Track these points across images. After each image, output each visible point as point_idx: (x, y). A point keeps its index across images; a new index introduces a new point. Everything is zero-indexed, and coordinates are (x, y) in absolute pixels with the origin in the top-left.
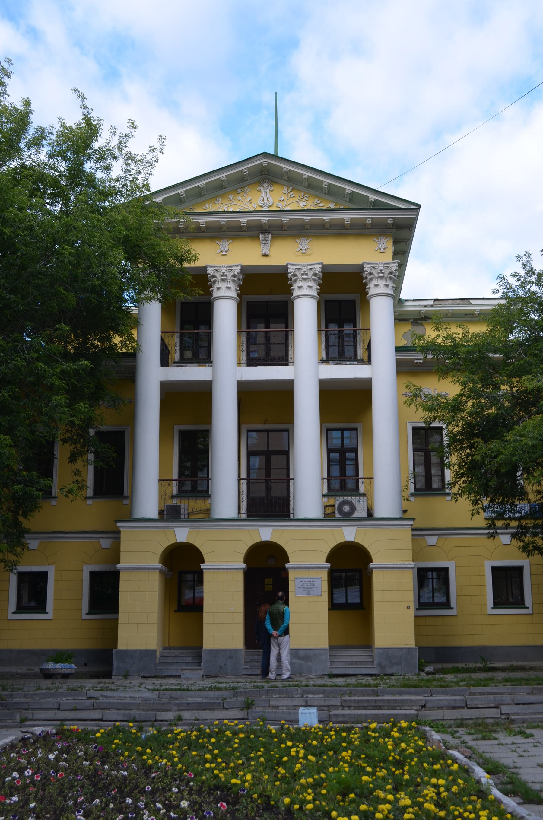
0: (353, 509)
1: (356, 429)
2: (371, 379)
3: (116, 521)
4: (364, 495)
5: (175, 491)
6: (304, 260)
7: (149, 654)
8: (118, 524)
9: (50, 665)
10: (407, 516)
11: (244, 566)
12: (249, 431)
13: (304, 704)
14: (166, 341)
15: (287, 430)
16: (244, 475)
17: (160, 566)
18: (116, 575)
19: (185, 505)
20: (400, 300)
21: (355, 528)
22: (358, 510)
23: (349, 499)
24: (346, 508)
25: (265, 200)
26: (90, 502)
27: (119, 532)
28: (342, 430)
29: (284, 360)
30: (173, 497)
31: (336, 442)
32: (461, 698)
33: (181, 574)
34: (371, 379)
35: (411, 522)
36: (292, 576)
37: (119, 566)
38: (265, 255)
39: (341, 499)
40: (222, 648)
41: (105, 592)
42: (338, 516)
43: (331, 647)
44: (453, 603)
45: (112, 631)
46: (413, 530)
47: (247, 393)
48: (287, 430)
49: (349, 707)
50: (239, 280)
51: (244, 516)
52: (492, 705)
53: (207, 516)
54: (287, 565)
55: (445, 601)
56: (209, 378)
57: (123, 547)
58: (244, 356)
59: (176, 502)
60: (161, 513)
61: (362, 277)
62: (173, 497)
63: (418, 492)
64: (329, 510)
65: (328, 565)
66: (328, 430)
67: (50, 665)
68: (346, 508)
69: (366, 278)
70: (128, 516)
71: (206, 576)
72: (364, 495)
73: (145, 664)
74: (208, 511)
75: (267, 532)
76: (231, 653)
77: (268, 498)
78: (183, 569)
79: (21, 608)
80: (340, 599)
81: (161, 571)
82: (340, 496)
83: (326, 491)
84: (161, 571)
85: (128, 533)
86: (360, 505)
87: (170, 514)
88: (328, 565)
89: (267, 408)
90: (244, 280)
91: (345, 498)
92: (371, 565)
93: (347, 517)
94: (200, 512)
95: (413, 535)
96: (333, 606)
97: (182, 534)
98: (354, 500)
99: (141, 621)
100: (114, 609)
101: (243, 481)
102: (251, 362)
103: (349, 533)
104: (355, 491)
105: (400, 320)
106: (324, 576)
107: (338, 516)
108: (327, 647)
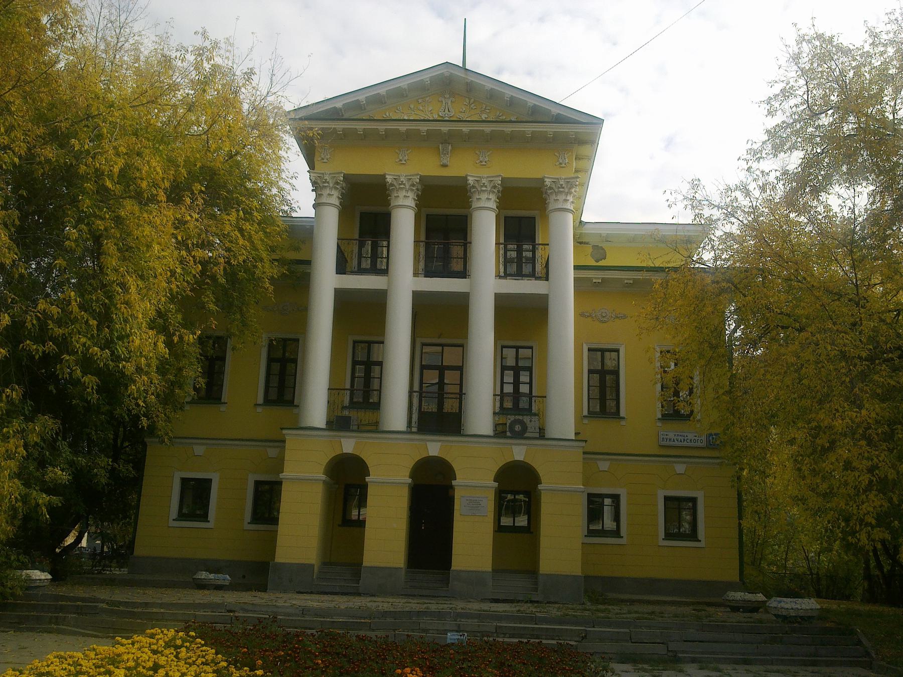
0: (525, 428)
1: (531, 348)
2: (547, 295)
3: (282, 429)
4: (535, 415)
5: (347, 402)
6: (485, 173)
7: (305, 568)
8: (284, 432)
9: (203, 575)
10: (580, 437)
11: (410, 481)
12: (423, 345)
13: (456, 628)
14: (342, 248)
15: (462, 346)
16: (416, 387)
17: (323, 477)
18: (279, 483)
19: (355, 415)
20: (581, 222)
21: (525, 447)
22: (529, 429)
23: (520, 418)
24: (518, 428)
25: (447, 111)
26: (259, 410)
27: (284, 441)
28: (517, 348)
29: (463, 274)
30: (344, 408)
31: (511, 362)
32: (628, 631)
33: (348, 487)
34: (547, 295)
35: (583, 444)
36: (458, 495)
37: (281, 476)
38: (445, 166)
39: (512, 418)
40: (382, 565)
41: (266, 501)
42: (508, 434)
43: (495, 571)
44: (624, 531)
45: (271, 541)
46: (584, 453)
47: (423, 305)
48: (462, 346)
49: (505, 634)
50: (418, 190)
51: (414, 430)
52: (658, 641)
53: (375, 427)
54: (454, 483)
55: (435, 410)
56: (385, 287)
57: (287, 457)
58: (422, 265)
59: (346, 413)
60: (329, 423)
61: (542, 192)
62: (344, 408)
63: (592, 414)
64: (500, 429)
65: (496, 484)
66: (503, 347)
67: (203, 575)
68: (518, 428)
69: (546, 193)
70: (297, 426)
71: (371, 491)
72: (535, 415)
73: (299, 579)
74: (377, 424)
75: (434, 447)
76: (390, 571)
77: (439, 413)
78: (347, 483)
79: (182, 516)
80: (506, 521)
81: (324, 482)
82: (511, 415)
83: (497, 410)
84: (324, 482)
85: (292, 439)
86: (532, 424)
87: (338, 423)
88: (496, 484)
89: (441, 321)
90: (423, 191)
91: (517, 417)
92: (540, 487)
93: (520, 435)
94: (368, 424)
95: (584, 459)
96: (499, 529)
97: (348, 445)
98: (526, 419)
99: (300, 533)
100: (275, 521)
101: (415, 394)
102: (429, 274)
103: (519, 452)
104: (529, 411)
105: (581, 243)
106: (491, 496)
107: (508, 434)
108: (490, 570)
